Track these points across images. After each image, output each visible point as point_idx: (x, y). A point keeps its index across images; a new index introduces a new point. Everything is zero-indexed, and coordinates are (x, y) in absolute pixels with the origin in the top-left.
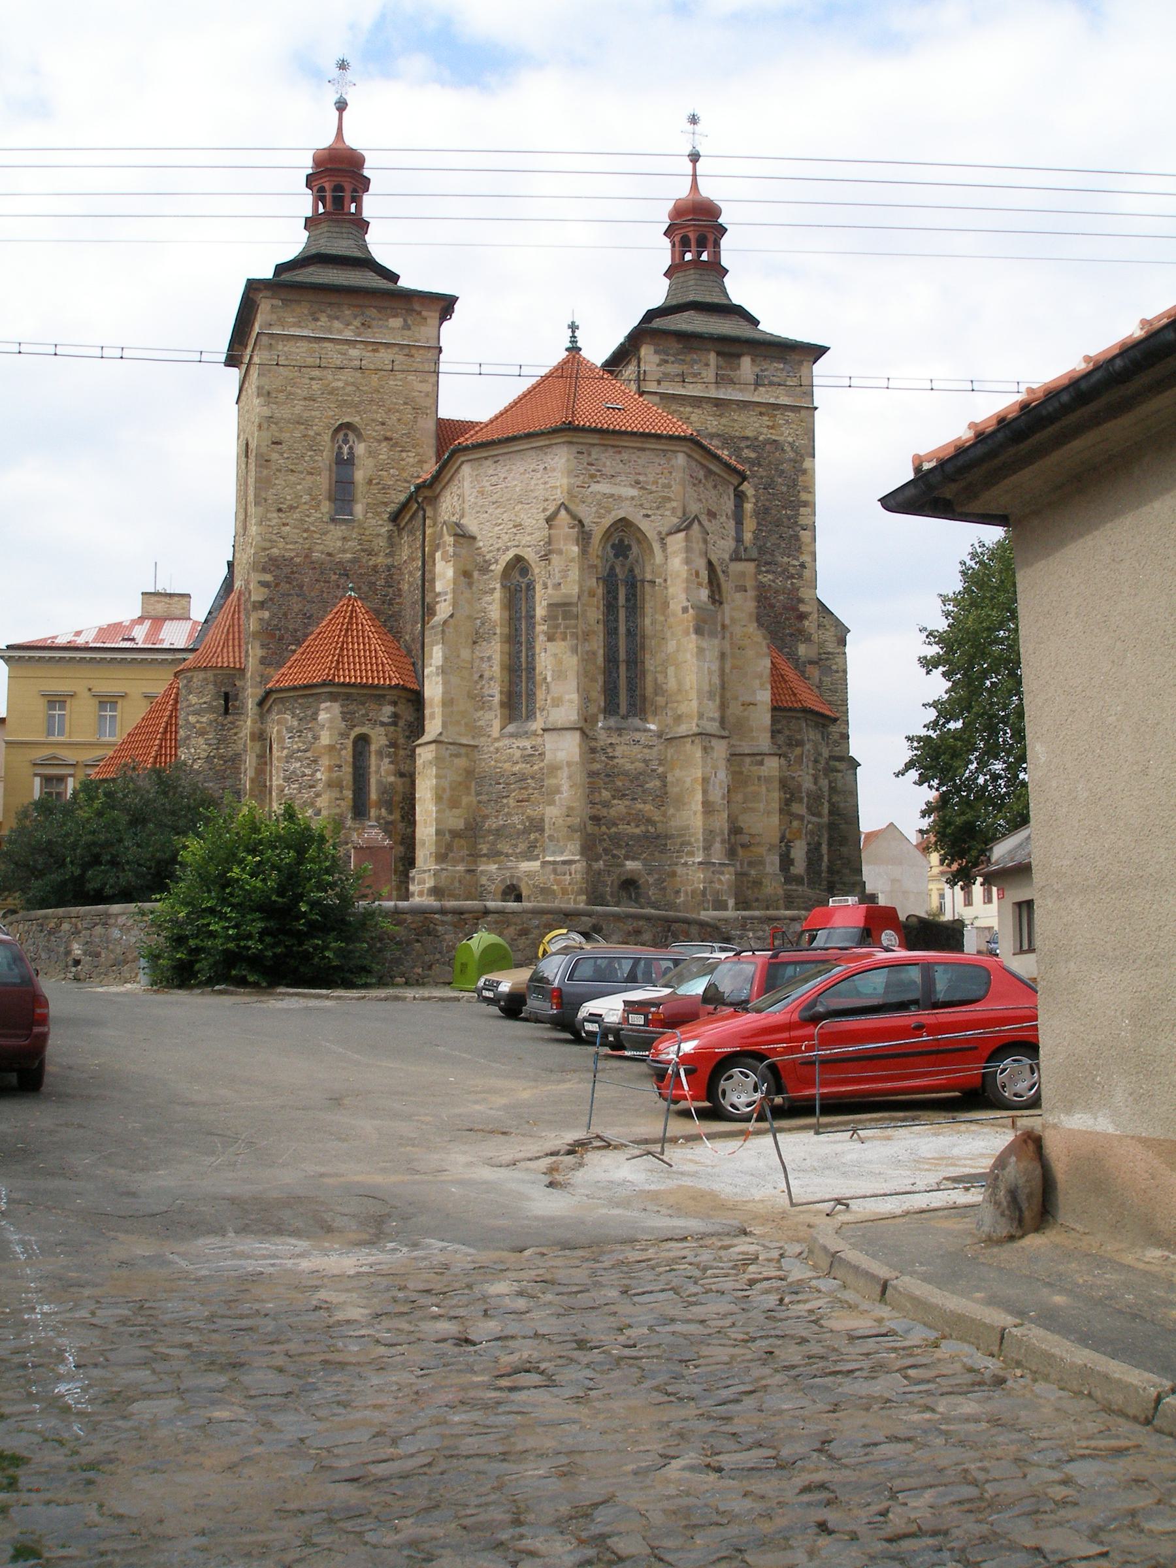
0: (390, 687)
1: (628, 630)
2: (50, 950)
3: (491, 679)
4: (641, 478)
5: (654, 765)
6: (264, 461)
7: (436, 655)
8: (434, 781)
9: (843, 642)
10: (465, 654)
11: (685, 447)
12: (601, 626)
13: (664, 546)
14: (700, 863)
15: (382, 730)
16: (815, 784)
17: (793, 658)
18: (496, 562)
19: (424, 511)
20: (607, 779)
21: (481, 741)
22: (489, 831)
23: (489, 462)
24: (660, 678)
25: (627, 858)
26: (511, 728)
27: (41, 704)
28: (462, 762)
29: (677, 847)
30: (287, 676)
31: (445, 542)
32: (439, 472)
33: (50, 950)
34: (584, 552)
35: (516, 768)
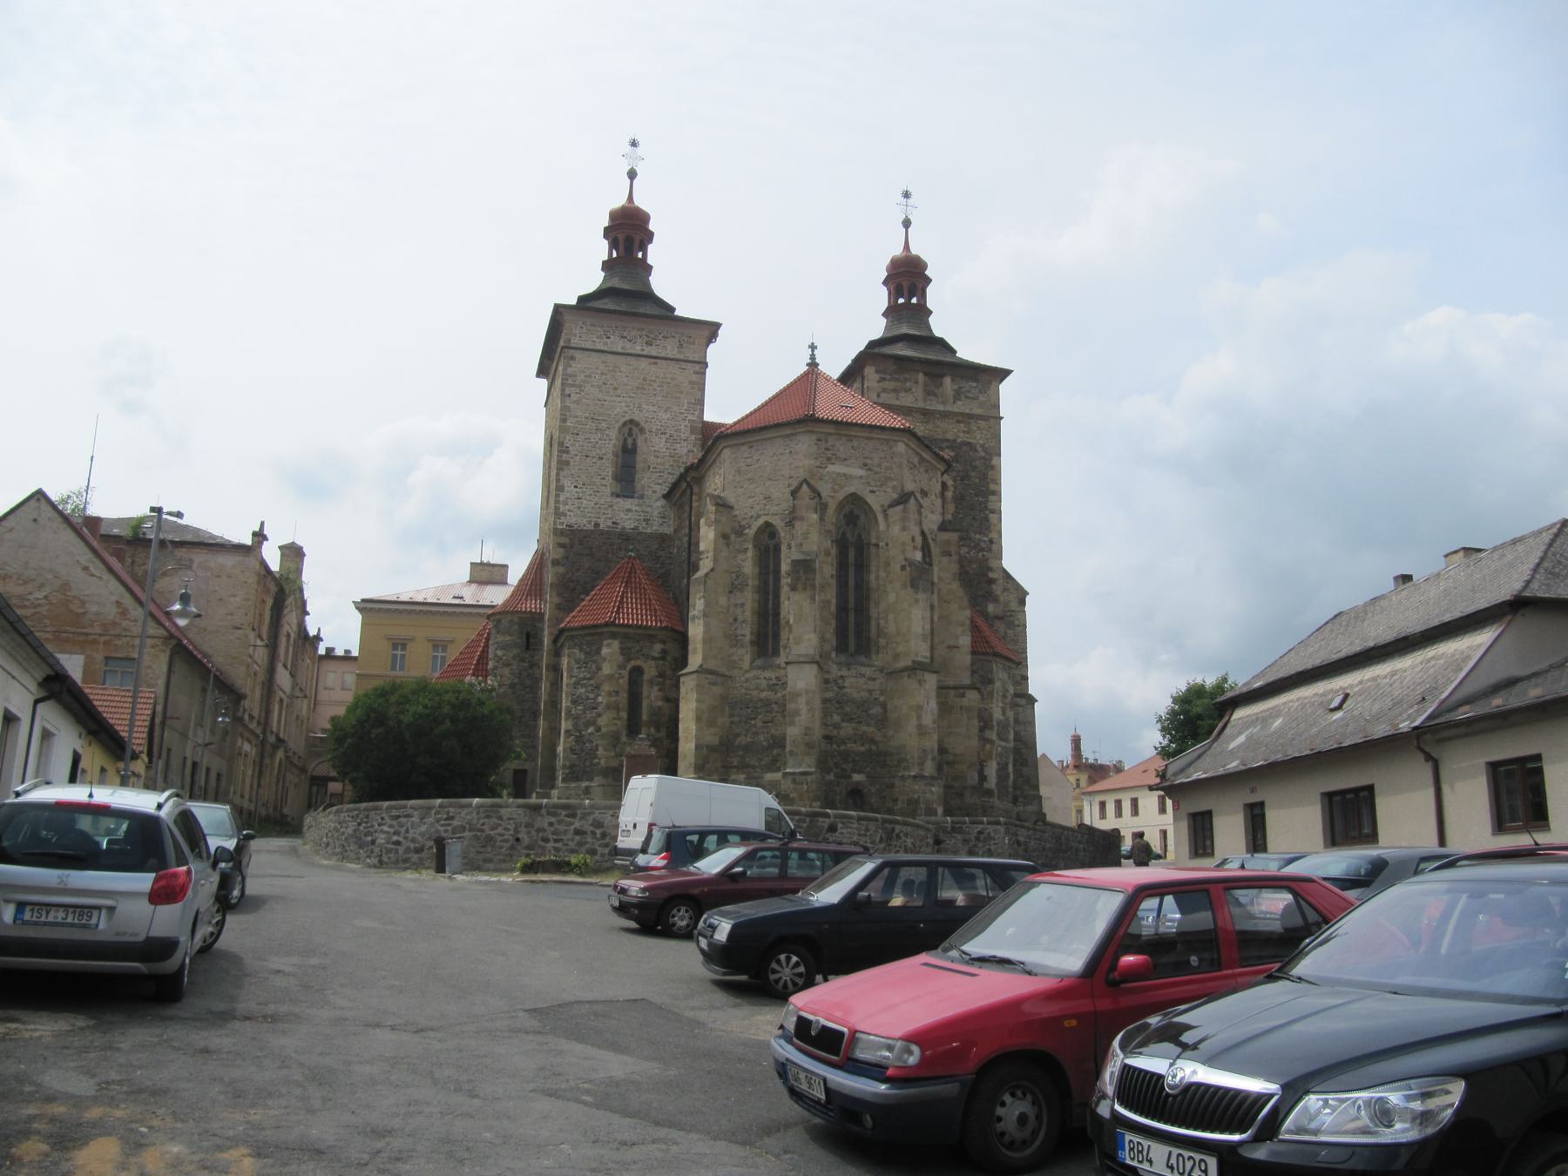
5: (876, 694)
6: (564, 449)
7: (698, 605)
9: (1022, 602)
10: (723, 601)
15: (652, 663)
17: (984, 614)
21: (735, 672)
23: (745, 448)
25: (854, 771)
28: (717, 690)
30: (575, 619)
32: (704, 456)
34: (821, 519)
35: (763, 695)
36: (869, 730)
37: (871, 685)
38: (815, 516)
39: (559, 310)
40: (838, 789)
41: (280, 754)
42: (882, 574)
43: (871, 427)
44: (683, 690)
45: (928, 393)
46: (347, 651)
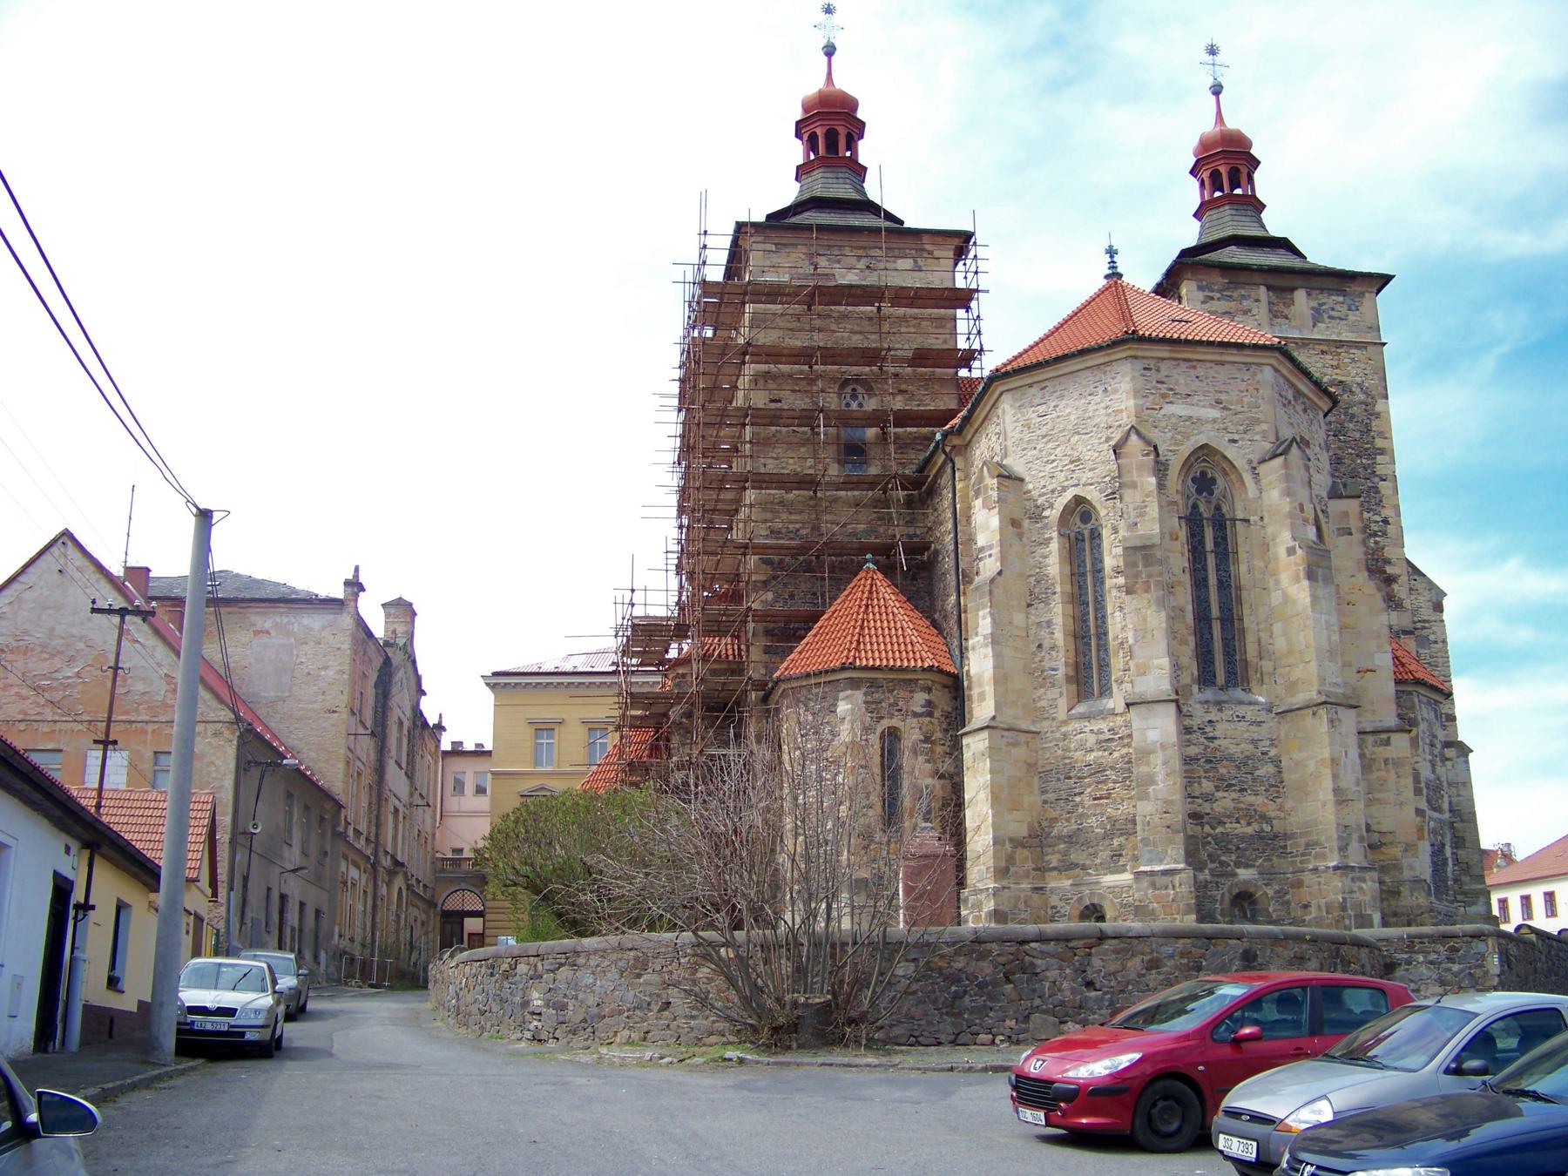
0: (923, 669)
1: (1220, 582)
2: (503, 1001)
3: (1052, 648)
4: (1223, 397)
5: (1264, 746)
7: (982, 623)
8: (989, 777)
9: (1439, 608)
10: (1019, 619)
11: (1273, 359)
12: (1188, 576)
13: (1256, 476)
14: (1336, 868)
16: (1434, 772)
18: (1051, 506)
19: (953, 462)
20: (1208, 766)
21: (1045, 726)
22: (1059, 838)
23: (1033, 390)
24: (1263, 636)
25: (1238, 864)
26: (1081, 709)
27: (528, 732)
28: (1021, 753)
29: (1301, 850)
31: (986, 487)
33: (503, 1001)
34: (1161, 486)
35: (1091, 757)
36: (1259, 801)
37: (1255, 732)
38: (1153, 480)
39: (740, 227)
40: (1218, 894)
41: (399, 882)
42: (1259, 564)
43: (1222, 344)
44: (967, 756)
45: (1275, 315)
46: (477, 745)
